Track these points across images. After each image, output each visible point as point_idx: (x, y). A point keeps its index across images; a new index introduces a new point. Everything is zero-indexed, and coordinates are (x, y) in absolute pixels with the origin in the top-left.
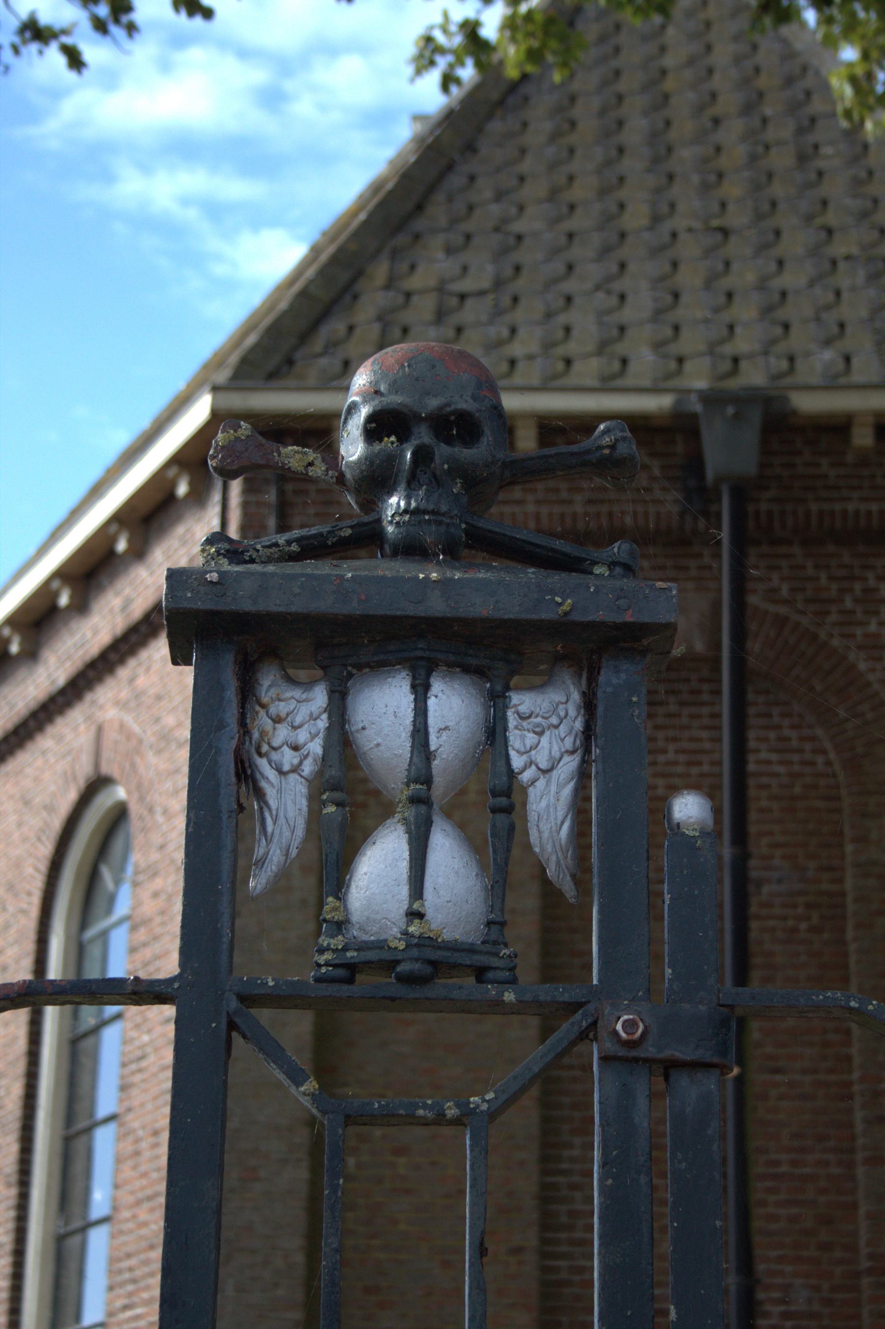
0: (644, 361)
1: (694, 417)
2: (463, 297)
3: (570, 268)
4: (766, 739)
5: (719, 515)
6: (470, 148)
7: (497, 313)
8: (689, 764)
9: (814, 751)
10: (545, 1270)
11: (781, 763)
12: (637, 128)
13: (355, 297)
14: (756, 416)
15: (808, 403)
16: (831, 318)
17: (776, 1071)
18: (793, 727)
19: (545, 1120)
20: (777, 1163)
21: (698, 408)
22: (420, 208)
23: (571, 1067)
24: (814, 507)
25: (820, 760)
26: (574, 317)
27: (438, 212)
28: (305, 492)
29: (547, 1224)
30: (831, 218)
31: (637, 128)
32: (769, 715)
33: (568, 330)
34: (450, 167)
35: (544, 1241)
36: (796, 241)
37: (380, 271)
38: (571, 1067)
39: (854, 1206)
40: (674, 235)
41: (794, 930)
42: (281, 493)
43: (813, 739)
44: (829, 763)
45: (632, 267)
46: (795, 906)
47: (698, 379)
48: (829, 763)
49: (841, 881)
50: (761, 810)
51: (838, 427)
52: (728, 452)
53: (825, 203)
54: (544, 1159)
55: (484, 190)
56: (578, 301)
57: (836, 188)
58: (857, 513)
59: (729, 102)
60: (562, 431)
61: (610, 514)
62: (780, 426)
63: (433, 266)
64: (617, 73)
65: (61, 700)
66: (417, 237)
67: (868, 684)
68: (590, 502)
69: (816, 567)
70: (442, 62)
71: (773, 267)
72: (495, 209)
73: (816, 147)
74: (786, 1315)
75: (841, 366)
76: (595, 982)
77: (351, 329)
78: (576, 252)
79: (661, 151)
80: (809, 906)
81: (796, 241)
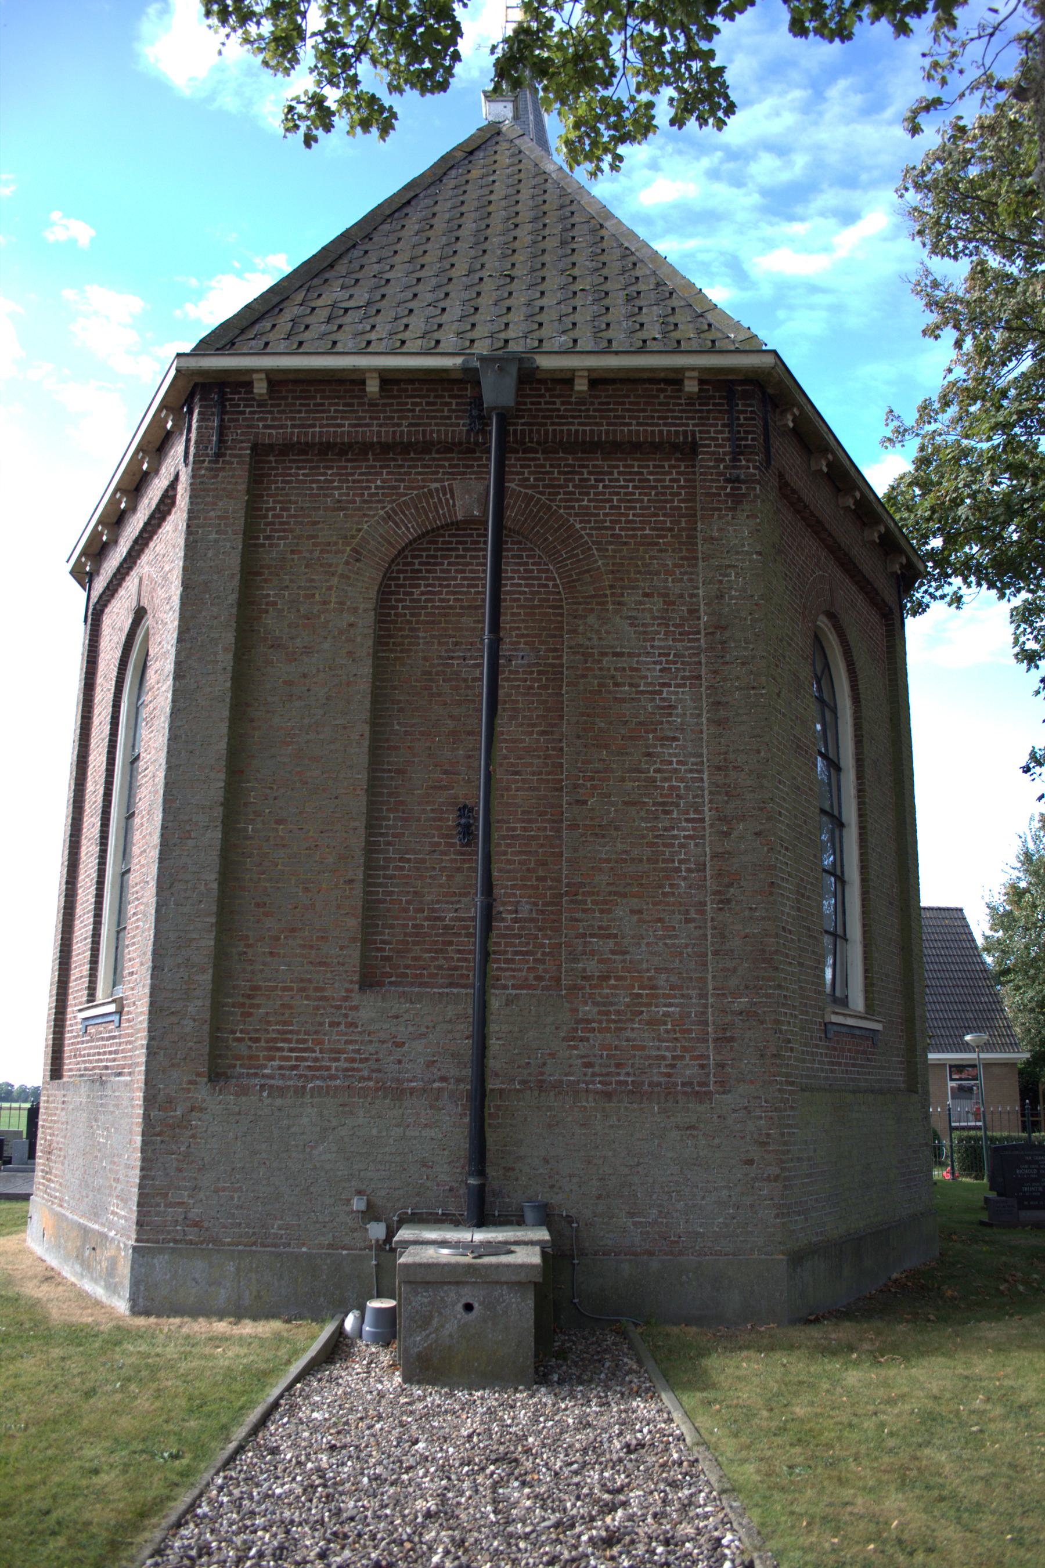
0: (449, 340)
1: (476, 370)
2: (346, 310)
3: (415, 295)
4: (519, 571)
5: (491, 432)
6: (369, 237)
7: (366, 317)
8: (469, 586)
9: (547, 579)
10: (367, 893)
11: (526, 586)
12: (469, 226)
13: (281, 310)
14: (513, 370)
15: (545, 362)
16: (568, 321)
17: (517, 773)
18: (533, 564)
19: (371, 804)
20: (514, 829)
21: (478, 364)
22: (331, 266)
23: (390, 771)
24: (550, 428)
25: (551, 583)
26: (412, 320)
27: (341, 268)
28: (237, 420)
29: (370, 866)
30: (576, 272)
31: (469, 226)
32: (521, 557)
33: (407, 326)
34: (354, 246)
35: (368, 876)
36: (554, 281)
37: (299, 297)
38: (390, 771)
39: (561, 854)
40: (481, 279)
41: (531, 687)
42: (222, 420)
43: (547, 571)
44: (556, 586)
45: (452, 295)
46: (532, 672)
47: (482, 348)
48: (556, 586)
49: (560, 657)
50: (513, 614)
51: (565, 380)
52: (498, 392)
53: (574, 264)
54: (369, 826)
55: (373, 257)
56: (416, 312)
57: (582, 258)
58: (577, 431)
59: (526, 215)
60: (397, 382)
61: (424, 432)
62: (529, 378)
63: (333, 294)
64: (463, 203)
65: (123, 571)
66: (326, 281)
67: (582, 537)
68: (410, 425)
69: (551, 466)
70: (303, 126)
71: (538, 295)
72: (376, 267)
73: (573, 238)
74: (515, 920)
75: (571, 345)
76: (930, 1056)
77: (274, 326)
78: (420, 288)
79: (481, 238)
80: (540, 673)
81: (554, 281)
